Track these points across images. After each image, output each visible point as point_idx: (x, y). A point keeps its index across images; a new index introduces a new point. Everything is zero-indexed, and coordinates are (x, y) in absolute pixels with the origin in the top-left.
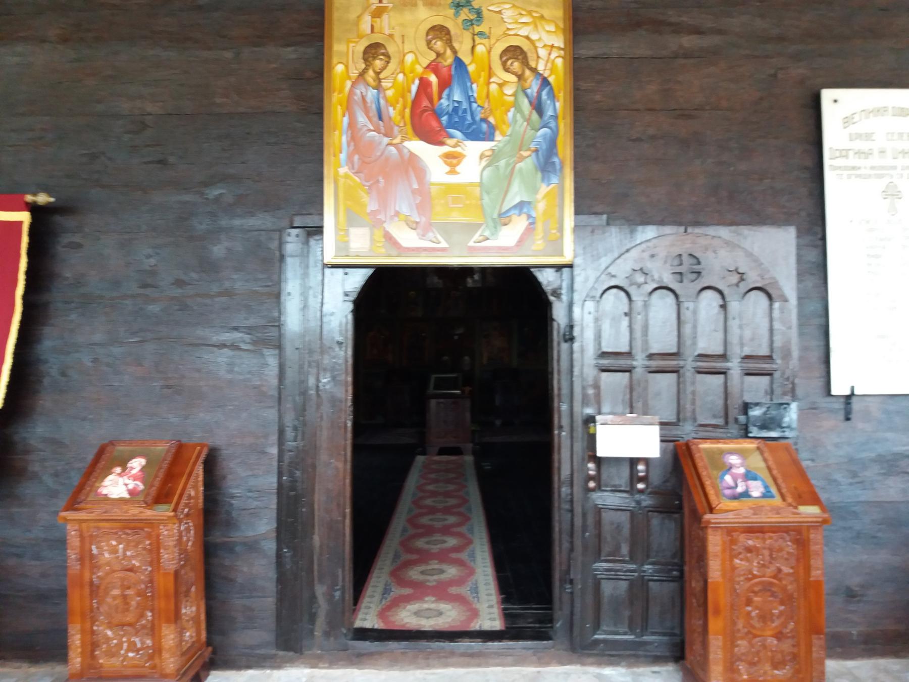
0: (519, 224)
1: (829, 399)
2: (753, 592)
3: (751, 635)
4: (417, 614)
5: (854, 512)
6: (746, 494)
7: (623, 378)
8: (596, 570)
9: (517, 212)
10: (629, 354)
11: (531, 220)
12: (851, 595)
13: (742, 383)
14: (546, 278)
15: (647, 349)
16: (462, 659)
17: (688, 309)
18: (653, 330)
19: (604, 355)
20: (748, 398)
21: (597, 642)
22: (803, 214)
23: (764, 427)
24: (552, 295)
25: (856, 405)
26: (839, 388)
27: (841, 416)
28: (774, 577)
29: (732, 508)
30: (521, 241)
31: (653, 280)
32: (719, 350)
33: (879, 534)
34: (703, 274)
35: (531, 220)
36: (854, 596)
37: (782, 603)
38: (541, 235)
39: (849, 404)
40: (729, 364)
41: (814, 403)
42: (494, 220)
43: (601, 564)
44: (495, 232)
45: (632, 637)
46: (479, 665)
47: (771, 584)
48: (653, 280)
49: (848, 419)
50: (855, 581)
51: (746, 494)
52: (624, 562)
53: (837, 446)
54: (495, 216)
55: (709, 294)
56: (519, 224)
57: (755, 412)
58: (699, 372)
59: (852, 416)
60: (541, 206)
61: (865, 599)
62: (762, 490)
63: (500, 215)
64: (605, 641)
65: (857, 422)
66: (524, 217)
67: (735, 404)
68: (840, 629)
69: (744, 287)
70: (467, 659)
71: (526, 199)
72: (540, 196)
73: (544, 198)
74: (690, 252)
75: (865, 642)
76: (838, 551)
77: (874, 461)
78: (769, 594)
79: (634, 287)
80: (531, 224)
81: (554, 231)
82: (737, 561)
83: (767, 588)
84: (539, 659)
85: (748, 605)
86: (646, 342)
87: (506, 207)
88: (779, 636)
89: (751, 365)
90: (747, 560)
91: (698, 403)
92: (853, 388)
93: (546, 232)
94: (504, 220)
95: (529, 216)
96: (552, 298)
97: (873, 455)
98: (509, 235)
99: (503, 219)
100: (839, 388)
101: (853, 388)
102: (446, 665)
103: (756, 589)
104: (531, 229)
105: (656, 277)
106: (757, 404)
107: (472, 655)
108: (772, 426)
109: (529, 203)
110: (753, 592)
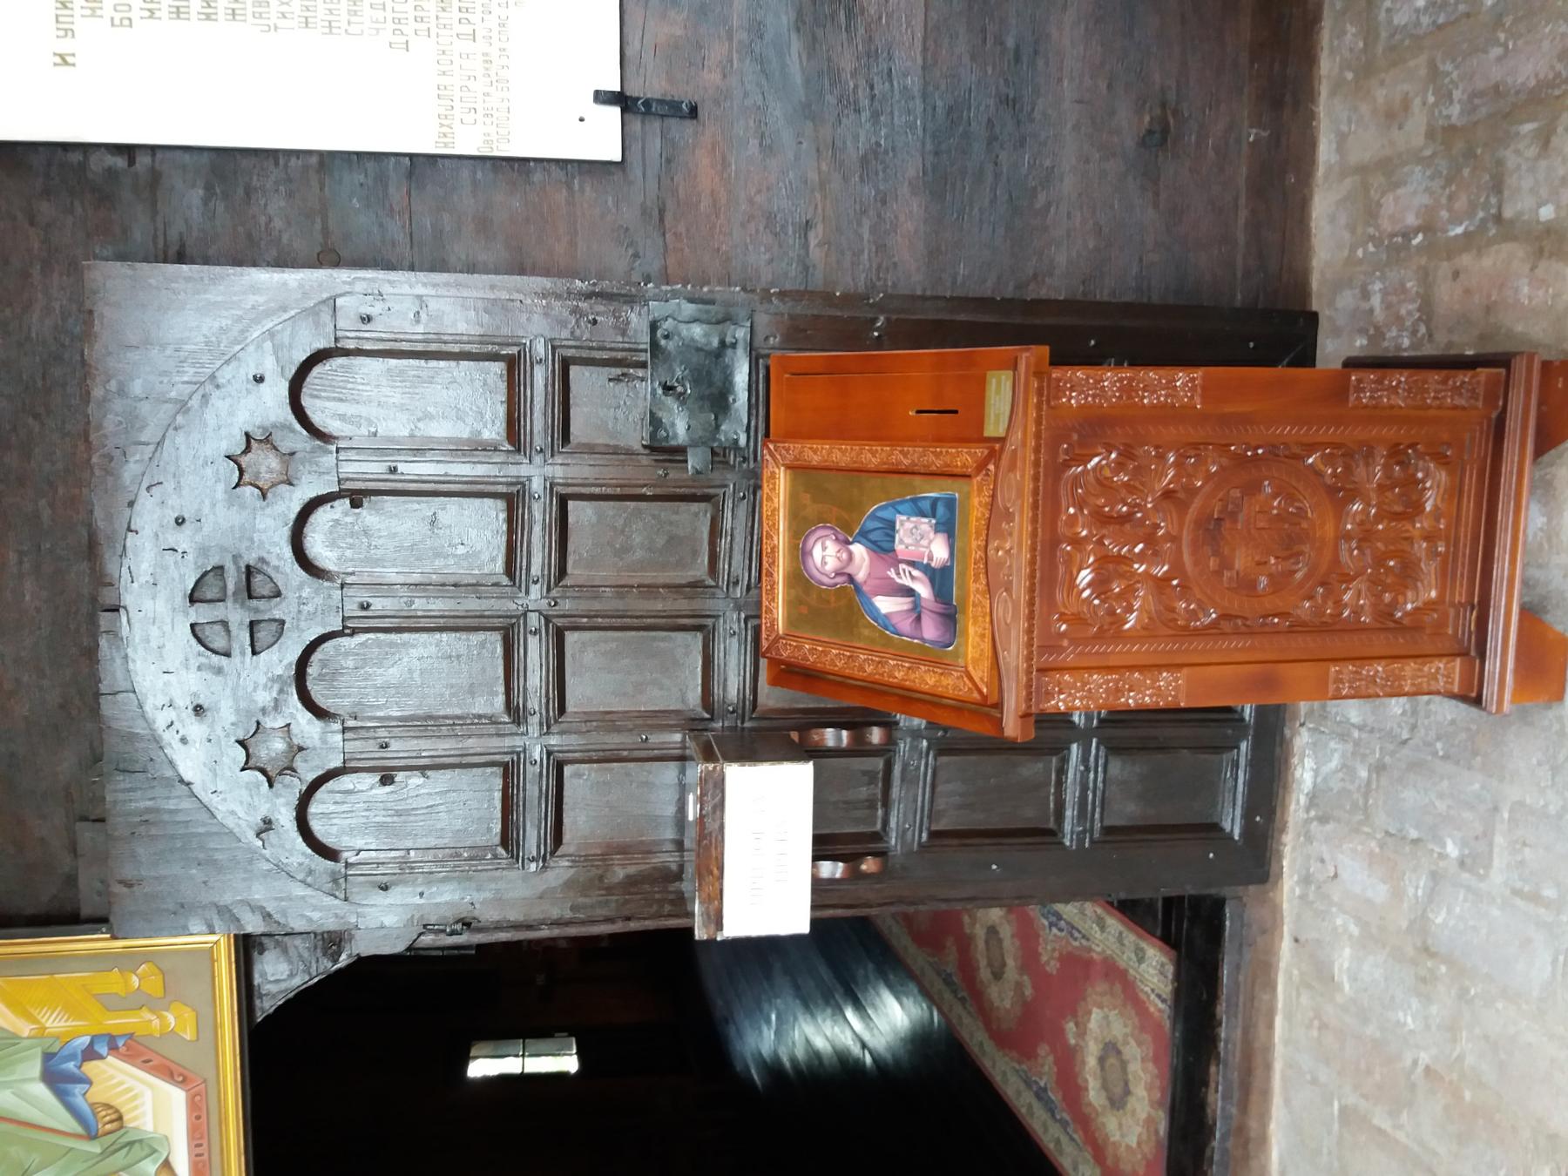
0: (116, 1079)
1: (636, 171)
2: (1218, 573)
3: (1333, 578)
4: (1118, 1102)
5: (950, 110)
6: (940, 578)
7: (577, 782)
8: (1081, 841)
9: (78, 1089)
10: (510, 772)
11: (103, 1049)
12: (1160, 136)
13: (590, 449)
14: (280, 977)
15: (493, 720)
16: (1254, 1109)
17: (365, 607)
18: (439, 698)
19: (509, 839)
20: (635, 436)
21: (1248, 827)
22: (45, 209)
23: (719, 401)
24: (335, 958)
25: (651, 86)
26: (601, 136)
27: (683, 130)
28: (1183, 507)
29: (986, 646)
30: (169, 1072)
31: (277, 705)
32: (494, 512)
33: (1010, 43)
34: (251, 558)
35: (103, 1049)
36: (1165, 130)
37: (1253, 488)
38: (146, 1015)
39: (647, 103)
40: (537, 486)
41: (645, 211)
42: (107, 1153)
43: (1067, 827)
44: (146, 1146)
45: (1244, 746)
46: (1268, 1067)
47: (1200, 523)
48: (277, 705)
49: (693, 112)
50: (1129, 123)
51: (940, 578)
52: (1062, 772)
53: (768, 149)
54: (95, 1148)
55: (317, 545)
56: (116, 1079)
57: (680, 426)
58: (562, 572)
59: (684, 93)
60: (55, 1023)
61: (1172, 96)
62: (925, 524)
63: (92, 1136)
64: (1248, 815)
65: (703, 83)
66: (91, 1068)
67: (646, 473)
68: (1242, 172)
69: (299, 439)
70: (1255, 1098)
71: (36, 1068)
72: (25, 1029)
73: (30, 1018)
74: (180, 600)
75: (1277, 104)
76: (1048, 163)
77: (812, 46)
78: (1227, 524)
79: (299, 763)
80: (113, 1048)
81: (135, 981)
82: (1132, 621)
83: (1212, 531)
84: (1264, 932)
85: (1253, 585)
86: (476, 448)
87: (68, 1123)
88: (1340, 494)
89: (539, 425)
90: (1128, 594)
91: (649, 577)
92: (602, 97)
93: (139, 1001)
94: (104, 1123)
95: (90, 1054)
96: (344, 960)
97: (796, 45)
98: (158, 1109)
99: (104, 1128)
100: (601, 136)
101: (602, 97)
102: (1263, 1140)
103: (1213, 563)
104: (131, 1048)
105: (264, 698)
106: (656, 422)
107: (1246, 1088)
108: (717, 377)
109: (48, 1057)
110: (1218, 573)
